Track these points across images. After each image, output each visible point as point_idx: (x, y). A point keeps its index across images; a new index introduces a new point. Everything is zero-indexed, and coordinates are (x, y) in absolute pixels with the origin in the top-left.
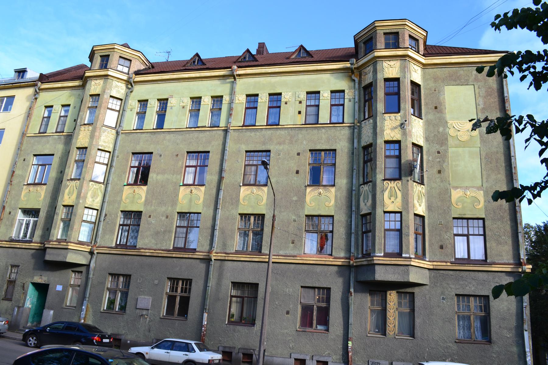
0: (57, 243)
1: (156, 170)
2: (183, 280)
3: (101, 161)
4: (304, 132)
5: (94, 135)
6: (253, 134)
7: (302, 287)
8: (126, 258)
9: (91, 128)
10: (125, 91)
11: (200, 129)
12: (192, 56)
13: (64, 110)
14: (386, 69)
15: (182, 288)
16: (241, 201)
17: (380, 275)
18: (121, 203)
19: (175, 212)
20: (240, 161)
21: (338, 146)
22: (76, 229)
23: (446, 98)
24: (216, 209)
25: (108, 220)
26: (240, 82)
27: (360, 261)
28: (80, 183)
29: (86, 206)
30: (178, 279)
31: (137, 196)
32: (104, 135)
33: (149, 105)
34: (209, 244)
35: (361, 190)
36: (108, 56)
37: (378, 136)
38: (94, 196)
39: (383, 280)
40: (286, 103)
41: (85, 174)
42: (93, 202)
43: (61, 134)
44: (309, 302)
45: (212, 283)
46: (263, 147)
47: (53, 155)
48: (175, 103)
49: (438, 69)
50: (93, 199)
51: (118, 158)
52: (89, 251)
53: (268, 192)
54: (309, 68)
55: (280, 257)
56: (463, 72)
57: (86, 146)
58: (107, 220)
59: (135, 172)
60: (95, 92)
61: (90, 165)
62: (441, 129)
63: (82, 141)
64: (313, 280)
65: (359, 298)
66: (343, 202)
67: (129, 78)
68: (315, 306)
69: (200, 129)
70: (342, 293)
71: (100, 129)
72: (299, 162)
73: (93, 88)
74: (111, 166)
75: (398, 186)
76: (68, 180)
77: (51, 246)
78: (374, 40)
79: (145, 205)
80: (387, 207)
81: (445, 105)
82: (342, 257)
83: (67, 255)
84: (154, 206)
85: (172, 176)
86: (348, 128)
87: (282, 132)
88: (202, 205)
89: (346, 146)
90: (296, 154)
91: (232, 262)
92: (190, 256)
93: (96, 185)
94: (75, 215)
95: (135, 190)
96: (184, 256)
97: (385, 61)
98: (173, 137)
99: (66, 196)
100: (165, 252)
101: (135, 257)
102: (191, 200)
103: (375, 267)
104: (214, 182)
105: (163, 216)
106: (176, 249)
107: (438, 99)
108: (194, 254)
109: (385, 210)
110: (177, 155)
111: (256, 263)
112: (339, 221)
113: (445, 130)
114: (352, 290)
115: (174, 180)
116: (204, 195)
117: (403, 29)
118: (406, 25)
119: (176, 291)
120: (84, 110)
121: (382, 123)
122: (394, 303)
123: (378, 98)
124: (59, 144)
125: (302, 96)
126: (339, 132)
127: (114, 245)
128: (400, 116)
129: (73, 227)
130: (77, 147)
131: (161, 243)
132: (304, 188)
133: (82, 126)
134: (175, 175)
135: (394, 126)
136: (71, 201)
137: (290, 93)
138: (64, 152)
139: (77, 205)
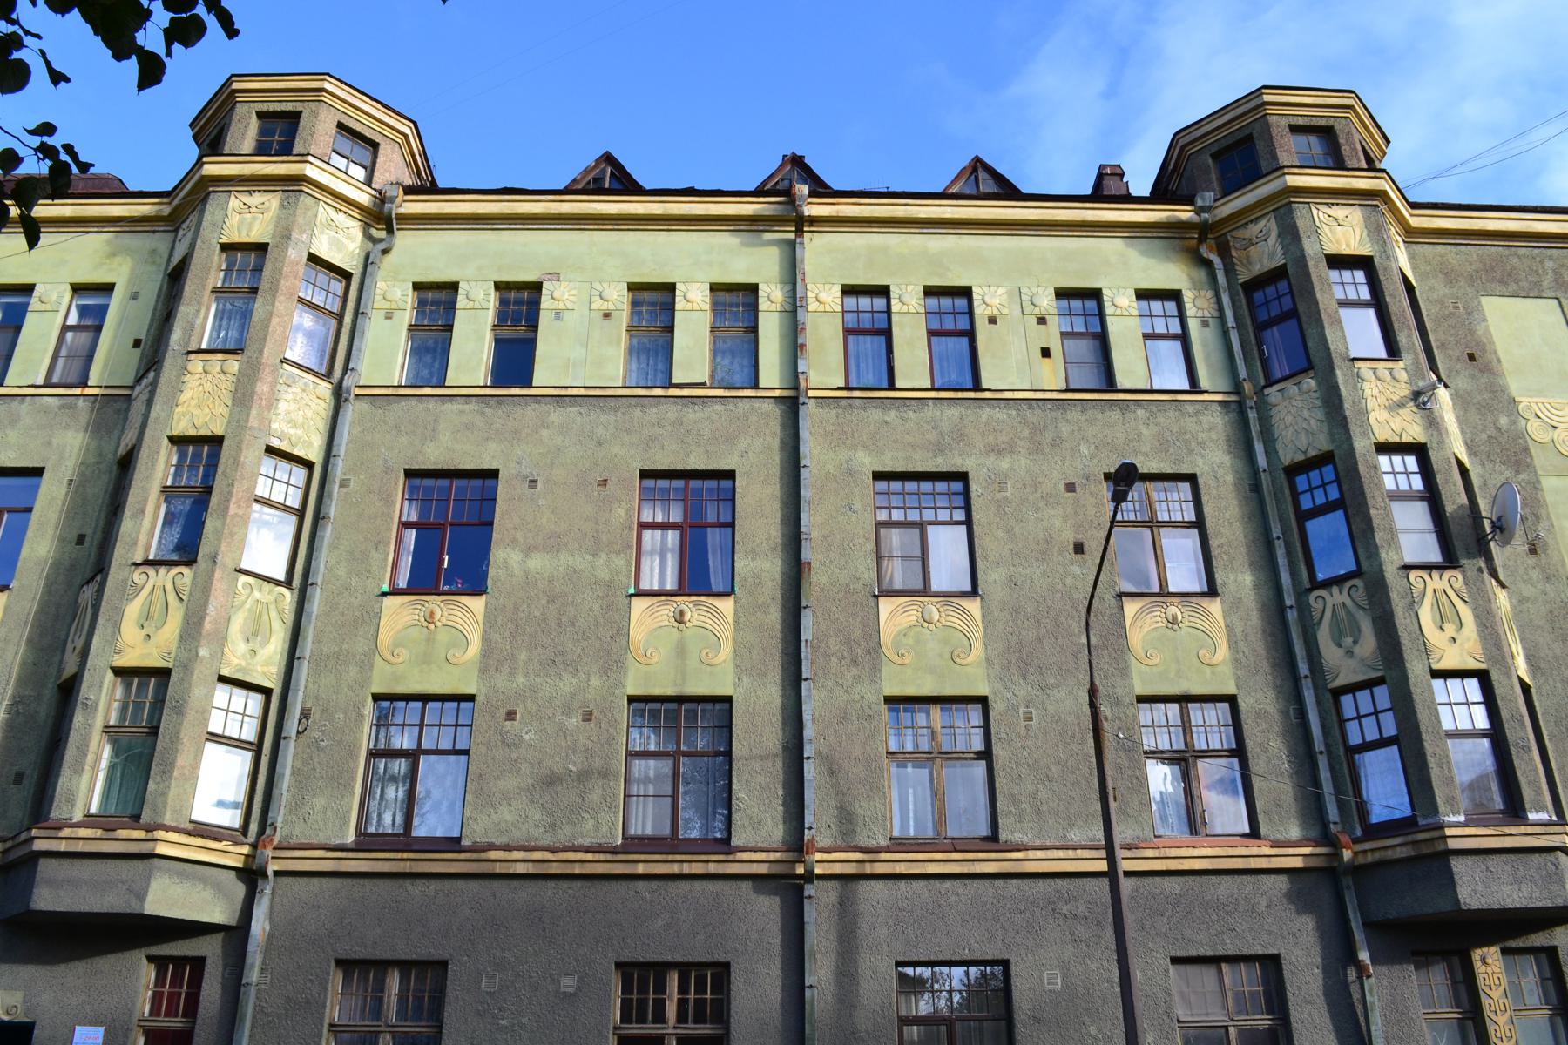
0: (99, 833)
1: (519, 535)
2: (684, 968)
3: (278, 497)
4: (1074, 414)
5: (253, 392)
6: (892, 416)
7: (1175, 961)
8: (415, 889)
9: (236, 365)
10: (361, 247)
11: (686, 392)
12: (590, 160)
13: (77, 306)
14: (1326, 228)
15: (682, 1004)
16: (887, 650)
17: (1475, 891)
18: (372, 667)
19: (622, 698)
20: (857, 505)
21: (1200, 464)
22: (183, 767)
23: (1492, 329)
24: (794, 679)
25: (317, 734)
26: (815, 246)
27: (1373, 850)
28: (195, 578)
29: (225, 672)
30: (662, 968)
31: (442, 637)
32: (290, 397)
33: (461, 301)
34: (784, 818)
35: (1316, 606)
36: (296, 116)
37: (1353, 428)
38: (255, 632)
39: (1486, 907)
40: (992, 320)
41: (219, 540)
42: (252, 658)
43: (78, 391)
44: (1207, 1014)
45: (820, 973)
46: (940, 460)
47: (38, 472)
48: (573, 299)
49: (1449, 247)
50: (251, 645)
51: (344, 490)
52: (240, 865)
53: (984, 616)
54: (1058, 215)
55: (1079, 852)
56: (1517, 259)
57: (219, 431)
58: (313, 733)
59: (412, 547)
60: (244, 233)
61: (239, 506)
62: (1503, 421)
63: (196, 412)
64: (1213, 932)
65: (1385, 983)
66: (1257, 646)
67: (381, 199)
68: (1232, 1030)
69: (686, 392)
70: (1325, 971)
71: (274, 371)
72: (1076, 512)
73: (233, 219)
74: (318, 518)
75: (1456, 586)
76: (136, 565)
77: (62, 846)
78: (1260, 146)
79: (484, 670)
80: (1438, 656)
81: (1495, 352)
82: (1294, 839)
83: (148, 886)
84: (526, 675)
85: (589, 557)
86: (1219, 409)
87: (1000, 414)
88: (730, 667)
89: (1228, 465)
90: (1062, 487)
91: (890, 883)
92: (712, 869)
93: (260, 590)
94: (180, 711)
95: (432, 614)
96: (687, 869)
97: (1317, 206)
98: (579, 419)
99: (130, 631)
100: (602, 857)
101: (461, 884)
102: (681, 651)
103: (1449, 861)
104: (770, 583)
105: (567, 712)
106: (636, 845)
107: (1472, 332)
108: (731, 858)
109: (1435, 667)
110: (604, 483)
111: (987, 882)
112: (1258, 714)
113: (1514, 423)
114: (1364, 956)
115: (604, 575)
116: (736, 630)
117: (1343, 121)
118: (1183, 148)
119: (660, 1017)
120: (202, 297)
121: (1355, 387)
122: (1502, 988)
123: (1322, 312)
124: (67, 427)
125: (1046, 302)
126: (1195, 419)
127: (350, 838)
128: (1405, 369)
129: (173, 763)
130: (175, 433)
131: (570, 822)
132: (1113, 602)
133: (192, 356)
134: (604, 556)
135: (1396, 398)
136: (155, 652)
137: (1001, 291)
138: (91, 459)
139: (185, 667)
